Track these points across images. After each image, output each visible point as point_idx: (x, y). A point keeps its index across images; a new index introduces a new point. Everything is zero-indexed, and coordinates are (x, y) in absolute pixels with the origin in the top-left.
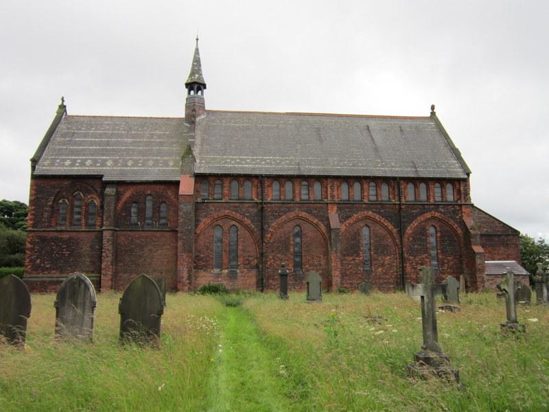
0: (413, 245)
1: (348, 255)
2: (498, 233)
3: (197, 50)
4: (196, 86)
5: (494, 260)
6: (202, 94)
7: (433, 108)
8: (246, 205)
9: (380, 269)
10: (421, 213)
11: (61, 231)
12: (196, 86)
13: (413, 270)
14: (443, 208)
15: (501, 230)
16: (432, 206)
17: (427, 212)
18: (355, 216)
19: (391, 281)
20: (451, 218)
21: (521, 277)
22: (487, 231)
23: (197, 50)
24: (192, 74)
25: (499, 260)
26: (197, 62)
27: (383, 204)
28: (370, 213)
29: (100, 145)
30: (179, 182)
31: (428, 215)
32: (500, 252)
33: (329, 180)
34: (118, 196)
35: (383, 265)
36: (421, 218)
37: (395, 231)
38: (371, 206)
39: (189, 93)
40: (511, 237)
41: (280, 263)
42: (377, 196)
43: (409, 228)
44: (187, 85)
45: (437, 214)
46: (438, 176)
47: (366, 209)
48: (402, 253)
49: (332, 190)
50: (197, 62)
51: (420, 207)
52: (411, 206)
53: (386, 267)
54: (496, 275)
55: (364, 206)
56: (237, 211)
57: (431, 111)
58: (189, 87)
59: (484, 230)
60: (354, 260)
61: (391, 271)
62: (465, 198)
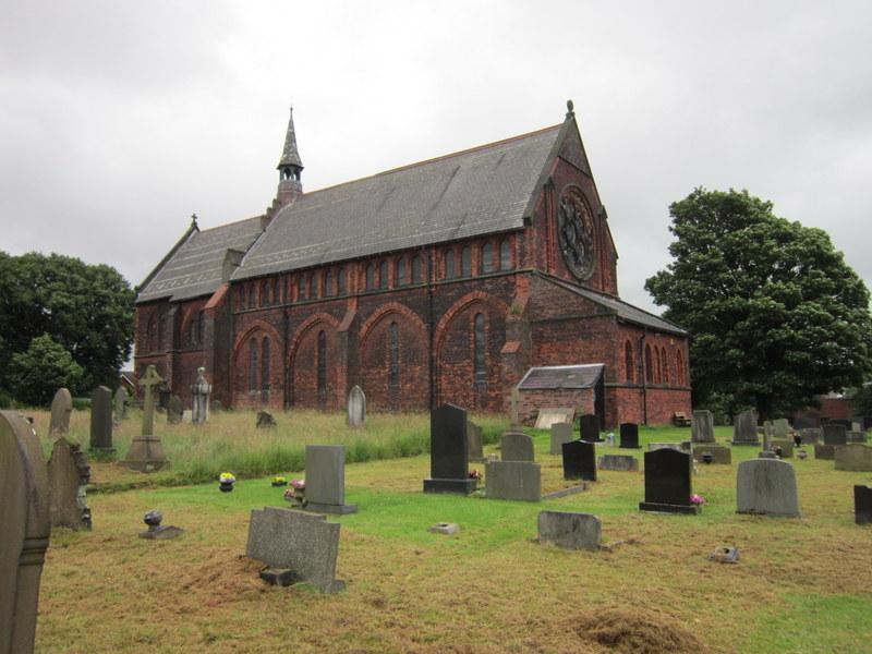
0: (452, 346)
1: (372, 367)
2: (574, 316)
3: (291, 122)
4: (291, 168)
5: (565, 364)
6: (298, 178)
7: (570, 105)
8: (274, 311)
9: (408, 385)
10: (460, 296)
11: (153, 356)
12: (291, 168)
13: (449, 386)
14: (491, 283)
15: (580, 309)
16: (476, 283)
17: (466, 294)
18: (378, 310)
19: (421, 402)
20: (502, 297)
21: (575, 393)
22: (555, 315)
23: (291, 122)
24: (286, 151)
25: (575, 363)
26: (291, 138)
27: (410, 289)
28: (395, 304)
29: (206, 264)
30: (650, 285)
31: (469, 298)
32: (577, 349)
33: (349, 267)
34: (180, 314)
35: (412, 380)
36: (460, 304)
37: (424, 327)
38: (397, 294)
39: (282, 178)
40: (597, 321)
41: (305, 378)
42: (515, 274)
43: (441, 322)
44: (280, 168)
45: (481, 295)
46: (480, 232)
47: (392, 299)
48: (432, 361)
49: (353, 277)
50: (291, 138)
51: (458, 286)
52: (447, 286)
53: (415, 383)
54: (533, 390)
55: (388, 295)
56: (265, 320)
57: (567, 111)
58: (283, 169)
59: (550, 312)
60: (379, 373)
61: (422, 388)
62: (521, 261)
